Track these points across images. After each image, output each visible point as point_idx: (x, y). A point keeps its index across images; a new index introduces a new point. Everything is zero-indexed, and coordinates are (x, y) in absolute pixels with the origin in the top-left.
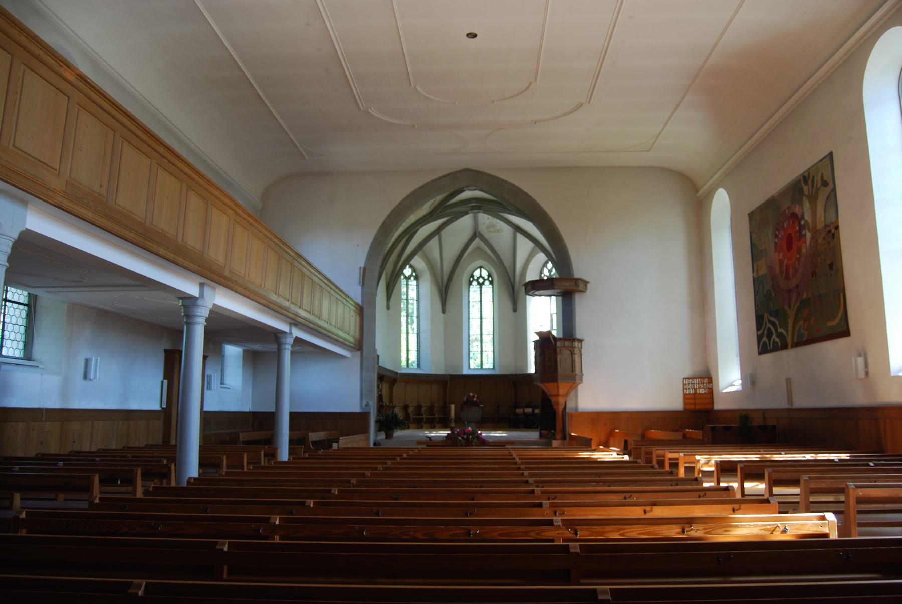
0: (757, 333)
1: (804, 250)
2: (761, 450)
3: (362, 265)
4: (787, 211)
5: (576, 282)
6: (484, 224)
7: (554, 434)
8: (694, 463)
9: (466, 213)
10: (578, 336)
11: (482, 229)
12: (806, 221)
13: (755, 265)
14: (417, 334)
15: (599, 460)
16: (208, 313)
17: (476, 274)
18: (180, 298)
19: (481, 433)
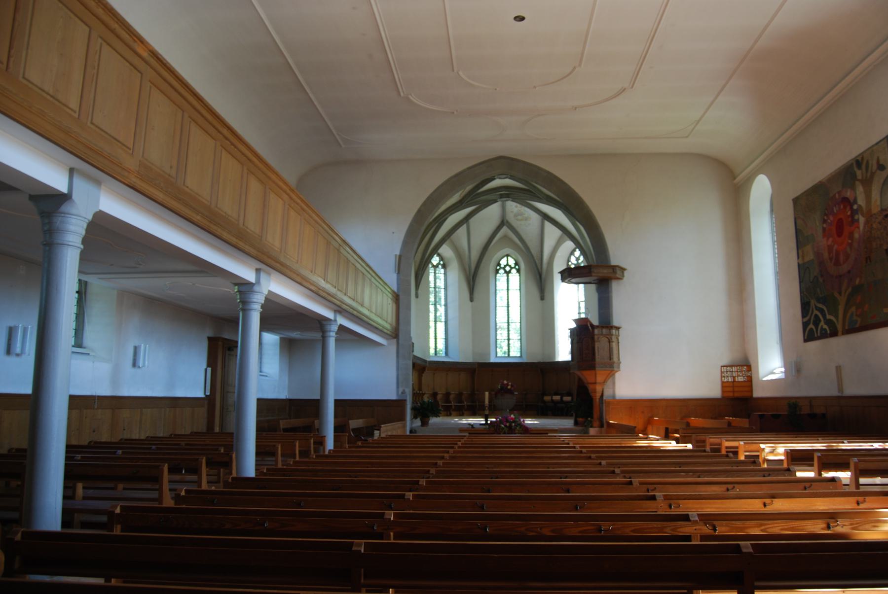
0: (803, 320)
1: (856, 236)
2: (819, 438)
3: (398, 253)
4: (837, 196)
5: (613, 269)
6: (512, 212)
7: (591, 422)
8: (758, 451)
9: (495, 201)
10: (615, 323)
11: (510, 218)
12: (860, 206)
13: (800, 252)
14: (445, 322)
15: (662, 448)
16: (264, 299)
17: (503, 262)
18: (236, 284)
19: (524, 421)
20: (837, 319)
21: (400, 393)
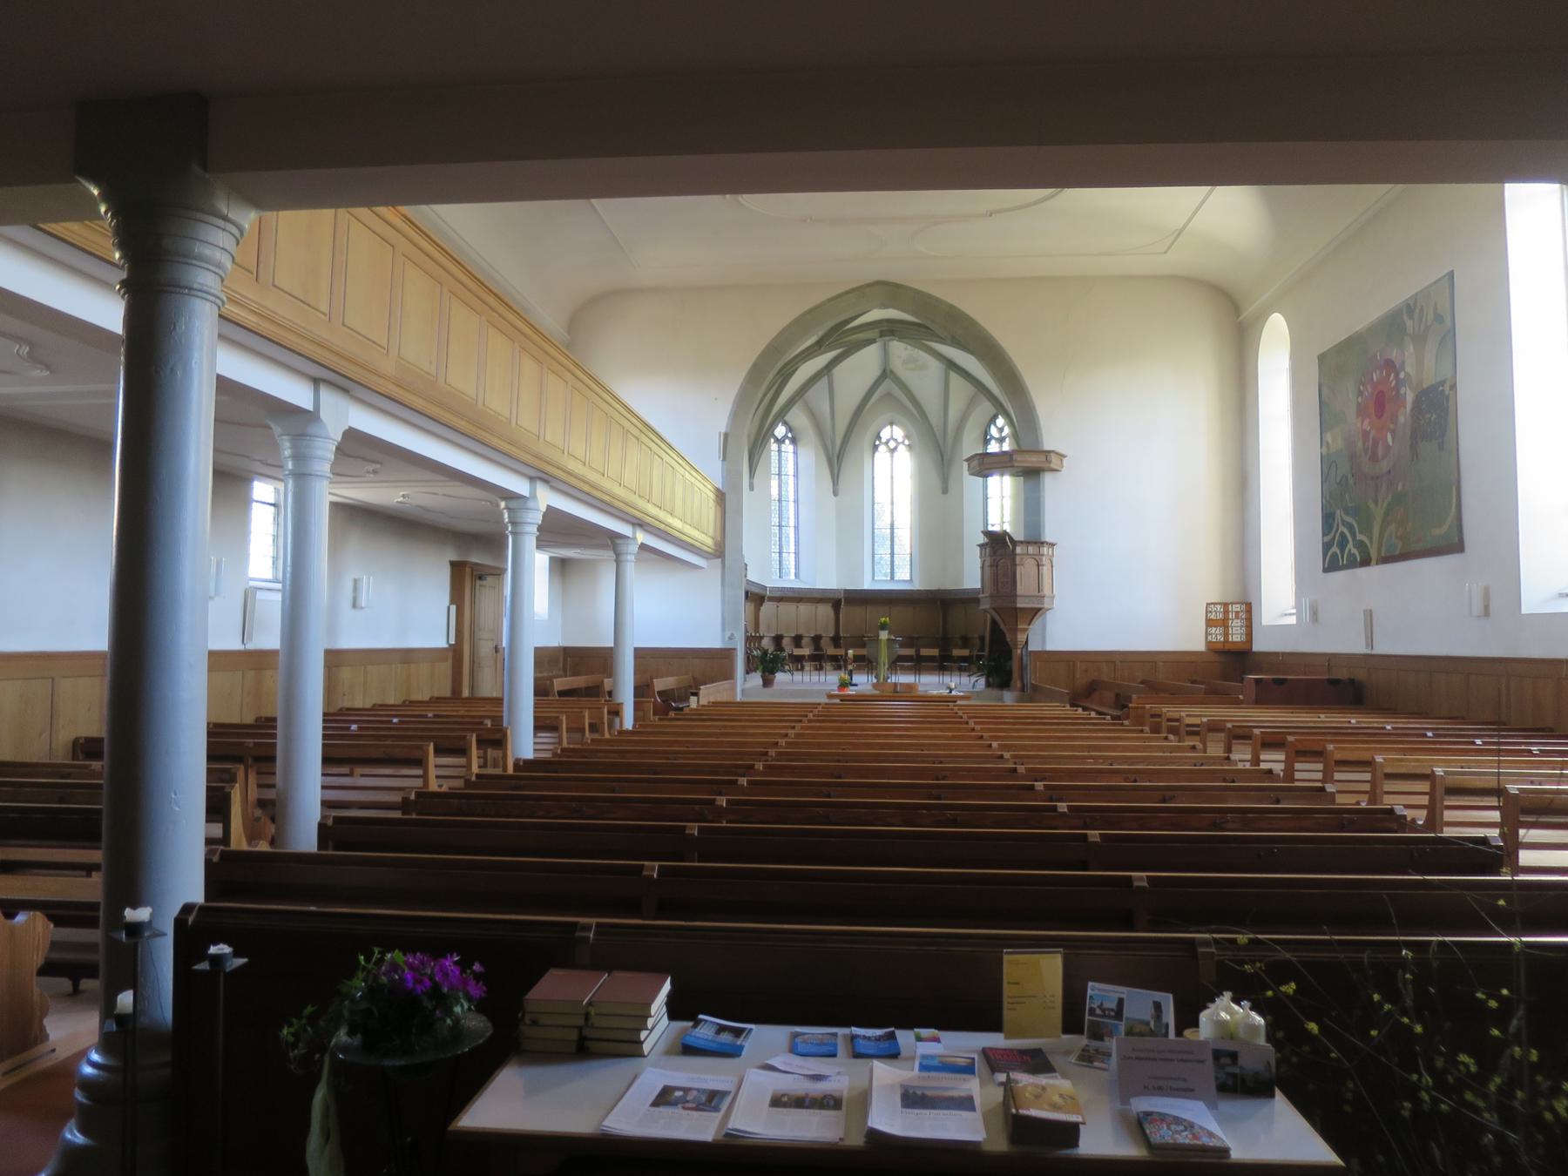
3: (723, 431)
10: (1048, 537)
11: (898, 367)
12: (1407, 373)
17: (885, 434)
20: (1371, 539)
21: (727, 638)
